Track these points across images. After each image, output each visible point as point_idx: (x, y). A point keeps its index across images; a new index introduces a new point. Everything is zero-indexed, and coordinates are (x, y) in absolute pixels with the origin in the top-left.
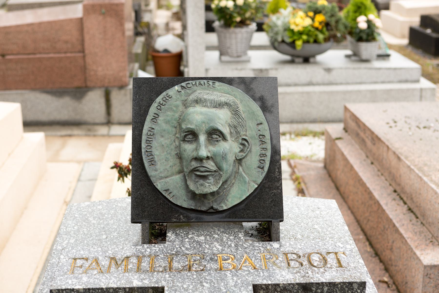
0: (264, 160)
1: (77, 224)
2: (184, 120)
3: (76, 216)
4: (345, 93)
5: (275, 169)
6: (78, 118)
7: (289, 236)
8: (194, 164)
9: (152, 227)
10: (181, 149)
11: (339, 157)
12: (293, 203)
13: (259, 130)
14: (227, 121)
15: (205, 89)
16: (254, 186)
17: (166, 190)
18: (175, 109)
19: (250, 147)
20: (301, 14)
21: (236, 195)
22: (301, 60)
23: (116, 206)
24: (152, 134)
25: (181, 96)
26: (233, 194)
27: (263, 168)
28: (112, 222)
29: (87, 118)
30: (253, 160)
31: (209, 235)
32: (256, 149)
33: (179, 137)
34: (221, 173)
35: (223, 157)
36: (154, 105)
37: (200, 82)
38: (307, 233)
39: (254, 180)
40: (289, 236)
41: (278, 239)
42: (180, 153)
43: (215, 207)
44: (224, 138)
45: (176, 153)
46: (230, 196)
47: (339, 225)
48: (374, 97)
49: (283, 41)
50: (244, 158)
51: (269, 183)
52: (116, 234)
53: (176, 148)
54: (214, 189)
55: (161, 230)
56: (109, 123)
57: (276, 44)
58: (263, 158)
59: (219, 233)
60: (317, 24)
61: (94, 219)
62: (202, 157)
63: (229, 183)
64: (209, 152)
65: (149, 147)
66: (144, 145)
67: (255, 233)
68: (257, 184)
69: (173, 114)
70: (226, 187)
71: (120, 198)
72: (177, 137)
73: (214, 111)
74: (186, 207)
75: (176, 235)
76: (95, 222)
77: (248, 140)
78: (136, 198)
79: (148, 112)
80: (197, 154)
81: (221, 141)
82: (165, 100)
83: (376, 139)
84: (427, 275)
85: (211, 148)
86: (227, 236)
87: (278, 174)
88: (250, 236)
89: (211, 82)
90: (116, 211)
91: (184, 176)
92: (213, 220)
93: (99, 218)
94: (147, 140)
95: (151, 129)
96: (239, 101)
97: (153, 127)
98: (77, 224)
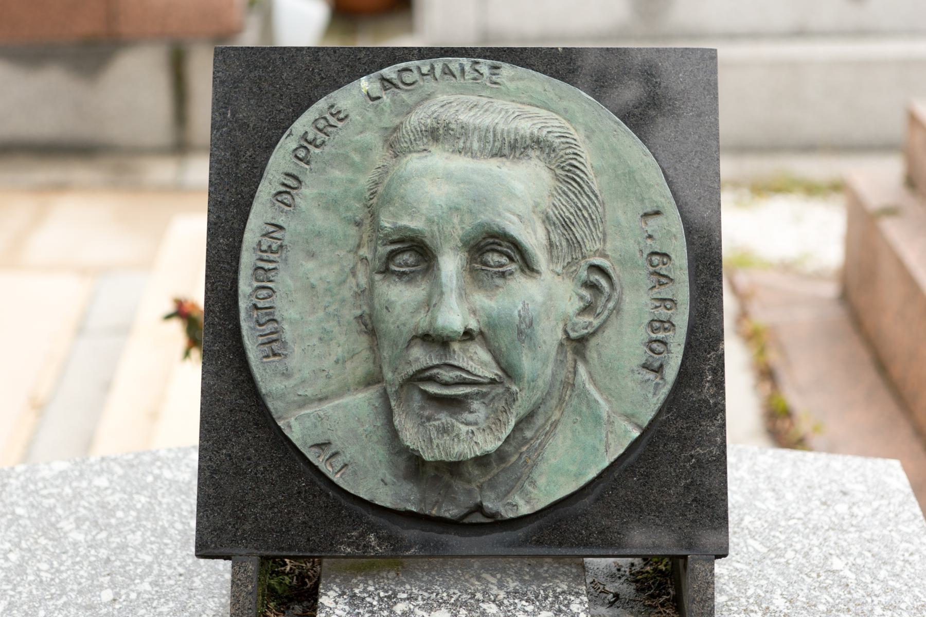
0: (663, 343)
1: (17, 545)
2: (387, 200)
3: (20, 511)
4: (906, 64)
5: (702, 375)
7: (743, 600)
8: (420, 357)
9: (270, 564)
10: (376, 301)
12: (756, 473)
13: (650, 237)
14: (537, 205)
15: (464, 90)
16: (626, 431)
17: (321, 446)
18: (356, 158)
19: (616, 295)
21: (563, 467)
23: (157, 478)
24: (275, 243)
25: (379, 112)
26: (553, 461)
27: (659, 370)
28: (136, 539)
29: (118, 131)
30: (625, 342)
31: (465, 604)
32: (636, 302)
33: (369, 257)
34: (514, 388)
35: (520, 332)
37: (446, 66)
38: (805, 587)
39: (629, 411)
40: (743, 600)
42: (370, 316)
43: (489, 505)
44: (528, 266)
45: (359, 312)
46: (543, 467)
47: (916, 557)
50: (593, 334)
51: (680, 423)
52: (148, 588)
53: (357, 295)
54: (489, 444)
55: (302, 577)
58: (660, 335)
59: (502, 595)
61: (78, 527)
62: (446, 333)
63: (539, 420)
64: (474, 312)
65: (264, 293)
66: (245, 286)
67: (627, 590)
68: (638, 426)
69: (350, 175)
70: (528, 434)
71: (170, 450)
72: (364, 259)
73: (494, 168)
74: (388, 505)
75: (350, 604)
76: (80, 537)
77: (611, 271)
78: (215, 472)
79: (263, 169)
80: (431, 323)
81: (518, 274)
82: (324, 128)
85: (480, 299)
86: (530, 608)
87: (712, 391)
88: (611, 604)
89: (484, 66)
90: (153, 496)
91: (385, 396)
92: (483, 552)
93: (96, 523)
94: (258, 268)
95: (271, 229)
96: (582, 131)
97: (281, 221)
98: (17, 545)
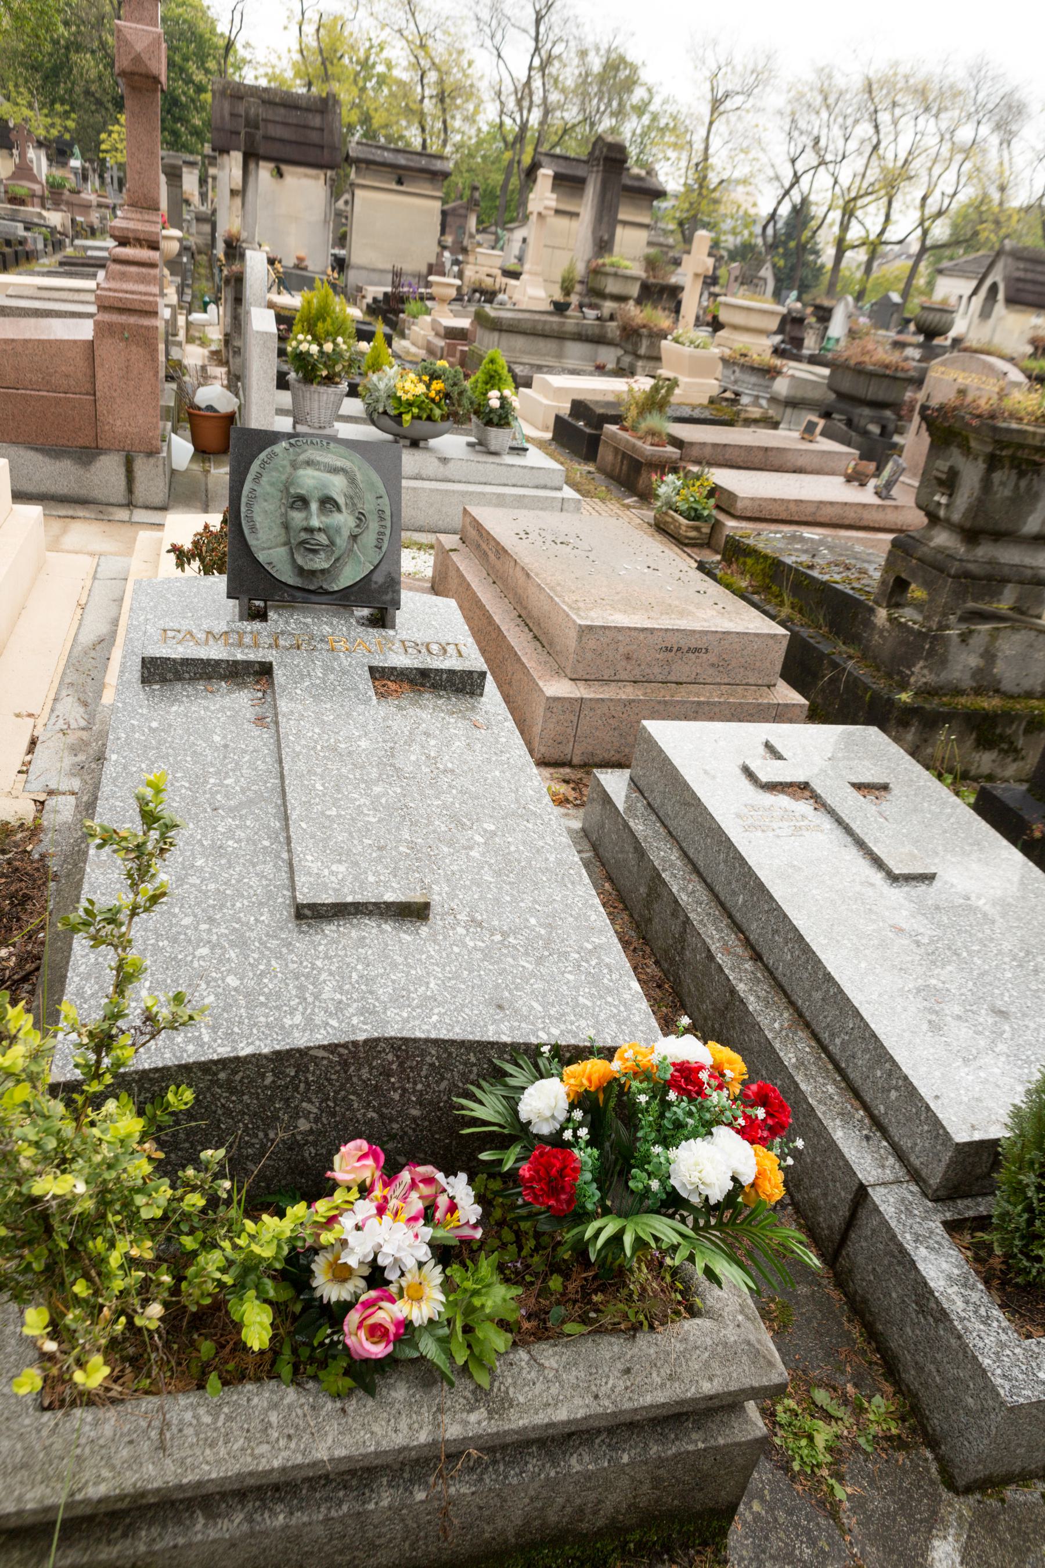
2: (292, 484)
4: (464, 494)
6: (83, 492)
8: (304, 535)
11: (452, 573)
20: (412, 376)
21: (348, 576)
22: (408, 442)
24: (253, 497)
29: (97, 494)
30: (369, 538)
32: (374, 526)
36: (257, 463)
41: (393, 627)
44: (339, 510)
48: (501, 501)
49: (385, 413)
56: (130, 504)
57: (375, 416)
60: (433, 394)
66: (243, 509)
83: (501, 551)
84: (549, 709)
